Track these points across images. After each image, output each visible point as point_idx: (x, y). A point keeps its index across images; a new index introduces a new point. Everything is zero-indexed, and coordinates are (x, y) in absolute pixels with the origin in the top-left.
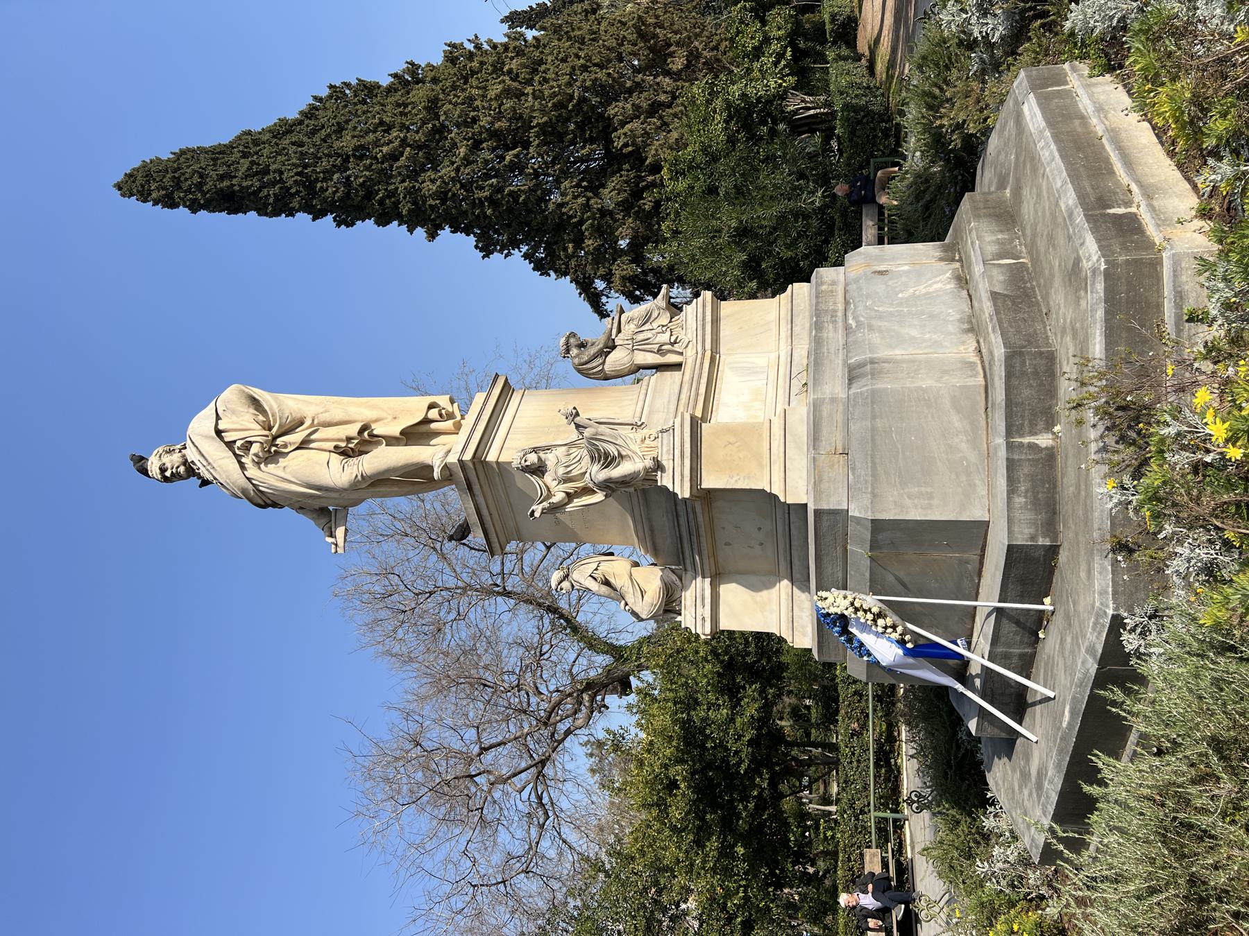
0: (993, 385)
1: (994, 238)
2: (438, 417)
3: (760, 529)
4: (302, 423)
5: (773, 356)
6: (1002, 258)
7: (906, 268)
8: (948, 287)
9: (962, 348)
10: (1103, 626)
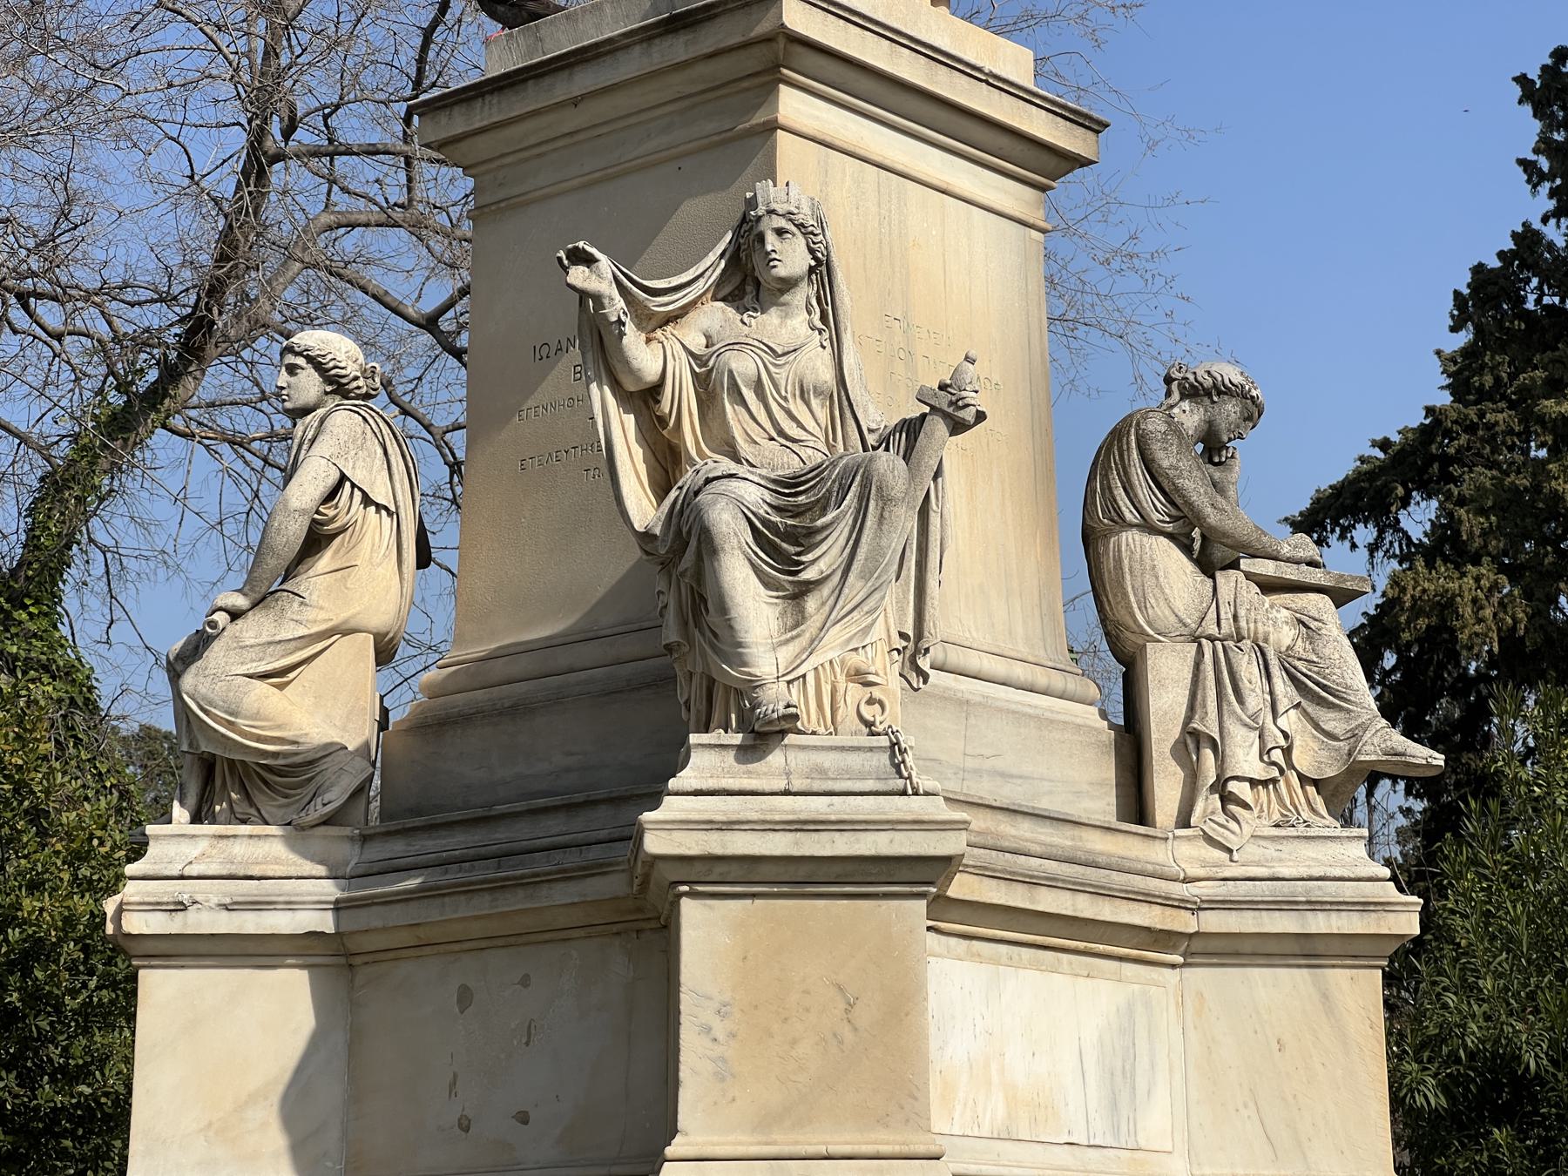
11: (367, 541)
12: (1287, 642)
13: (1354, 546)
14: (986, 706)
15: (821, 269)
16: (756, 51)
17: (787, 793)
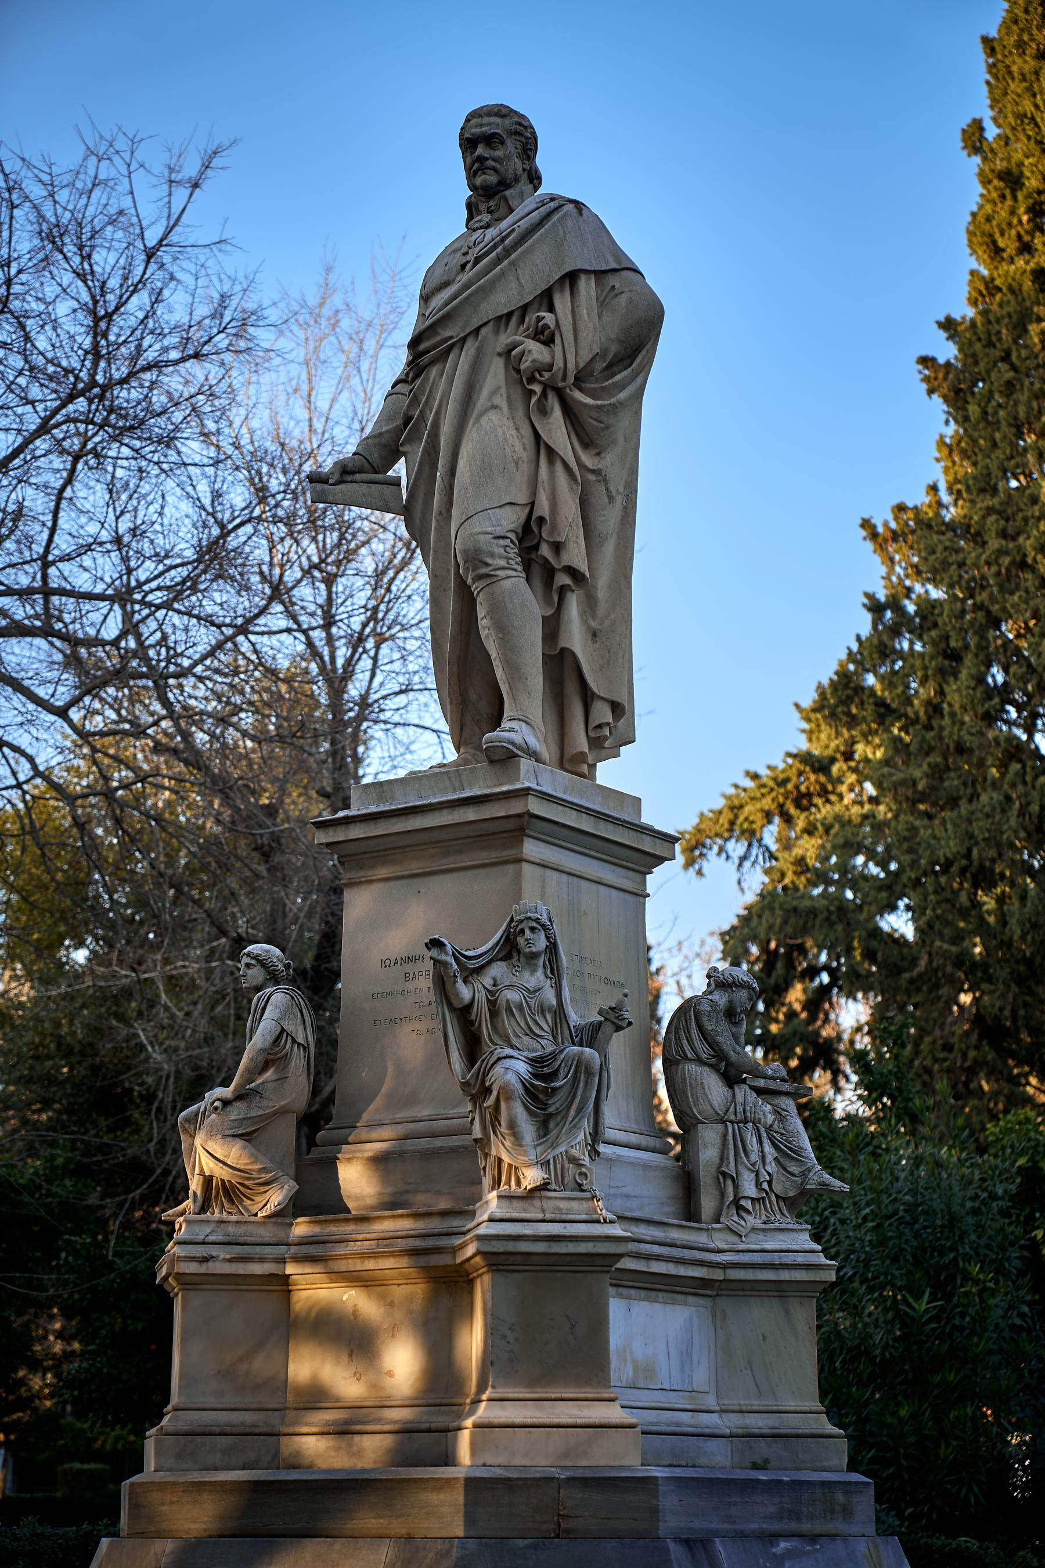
5: (711, 1402)
11: (293, 1063)
12: (770, 1122)
13: (728, 858)
15: (552, 948)
16: (512, 820)
17: (543, 1221)
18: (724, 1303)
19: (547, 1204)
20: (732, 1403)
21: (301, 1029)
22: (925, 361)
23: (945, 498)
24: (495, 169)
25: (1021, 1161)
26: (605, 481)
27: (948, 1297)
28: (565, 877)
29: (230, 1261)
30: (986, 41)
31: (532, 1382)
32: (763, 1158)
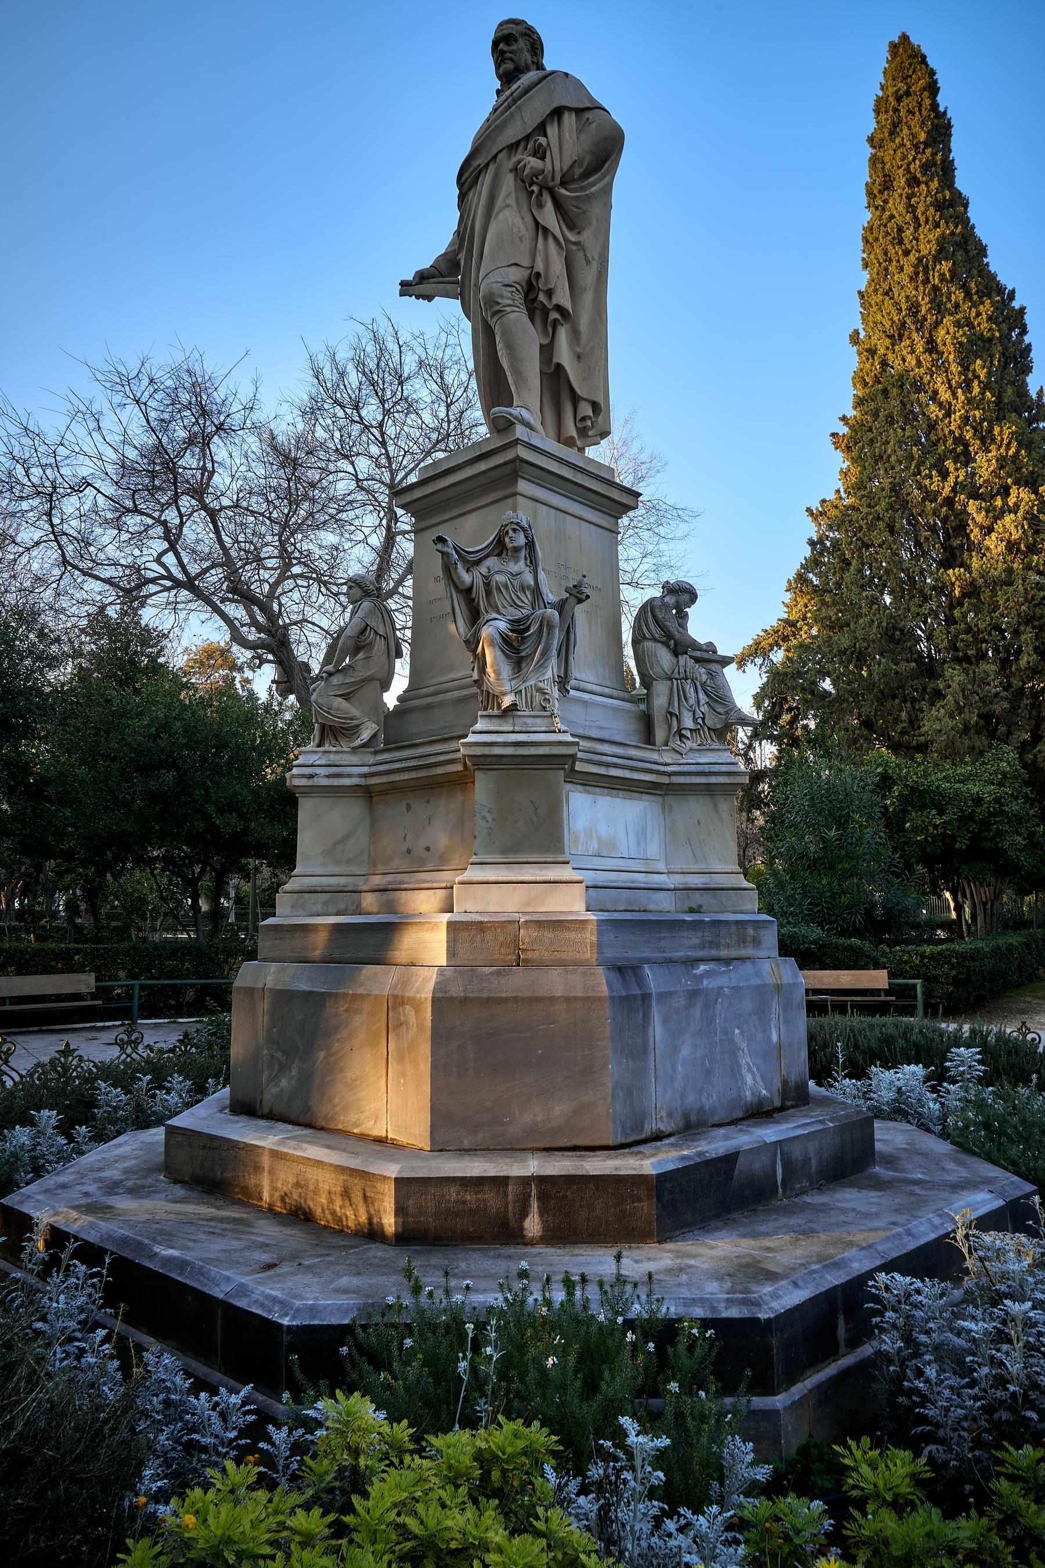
0: (609, 1157)
1: (812, 1154)
2: (579, 416)
3: (428, 849)
4: (571, 228)
5: (661, 867)
6: (783, 1166)
7: (775, 1038)
8: (748, 1094)
9: (663, 1113)
10: (270, 1311)
14: (594, 703)
15: (530, 545)
18: (670, 799)
19: (518, 721)
20: (677, 867)
21: (381, 626)
22: (833, 435)
23: (843, 495)
24: (511, 59)
25: (879, 770)
26: (584, 250)
27: (844, 829)
28: (553, 511)
29: (328, 776)
30: (859, 292)
31: (505, 851)
32: (698, 702)
